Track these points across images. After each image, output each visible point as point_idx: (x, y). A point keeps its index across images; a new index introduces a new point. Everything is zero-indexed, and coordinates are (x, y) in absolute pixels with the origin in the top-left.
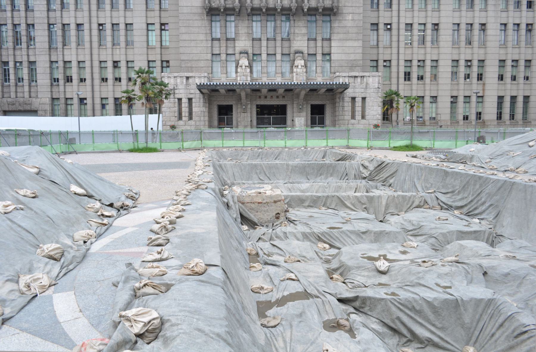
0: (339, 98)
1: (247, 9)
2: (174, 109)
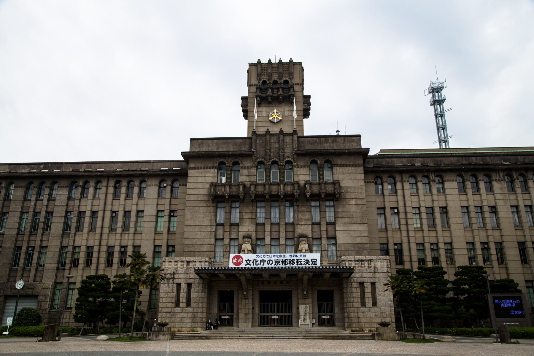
0: (347, 283)
1: (251, 196)
2: (172, 294)
